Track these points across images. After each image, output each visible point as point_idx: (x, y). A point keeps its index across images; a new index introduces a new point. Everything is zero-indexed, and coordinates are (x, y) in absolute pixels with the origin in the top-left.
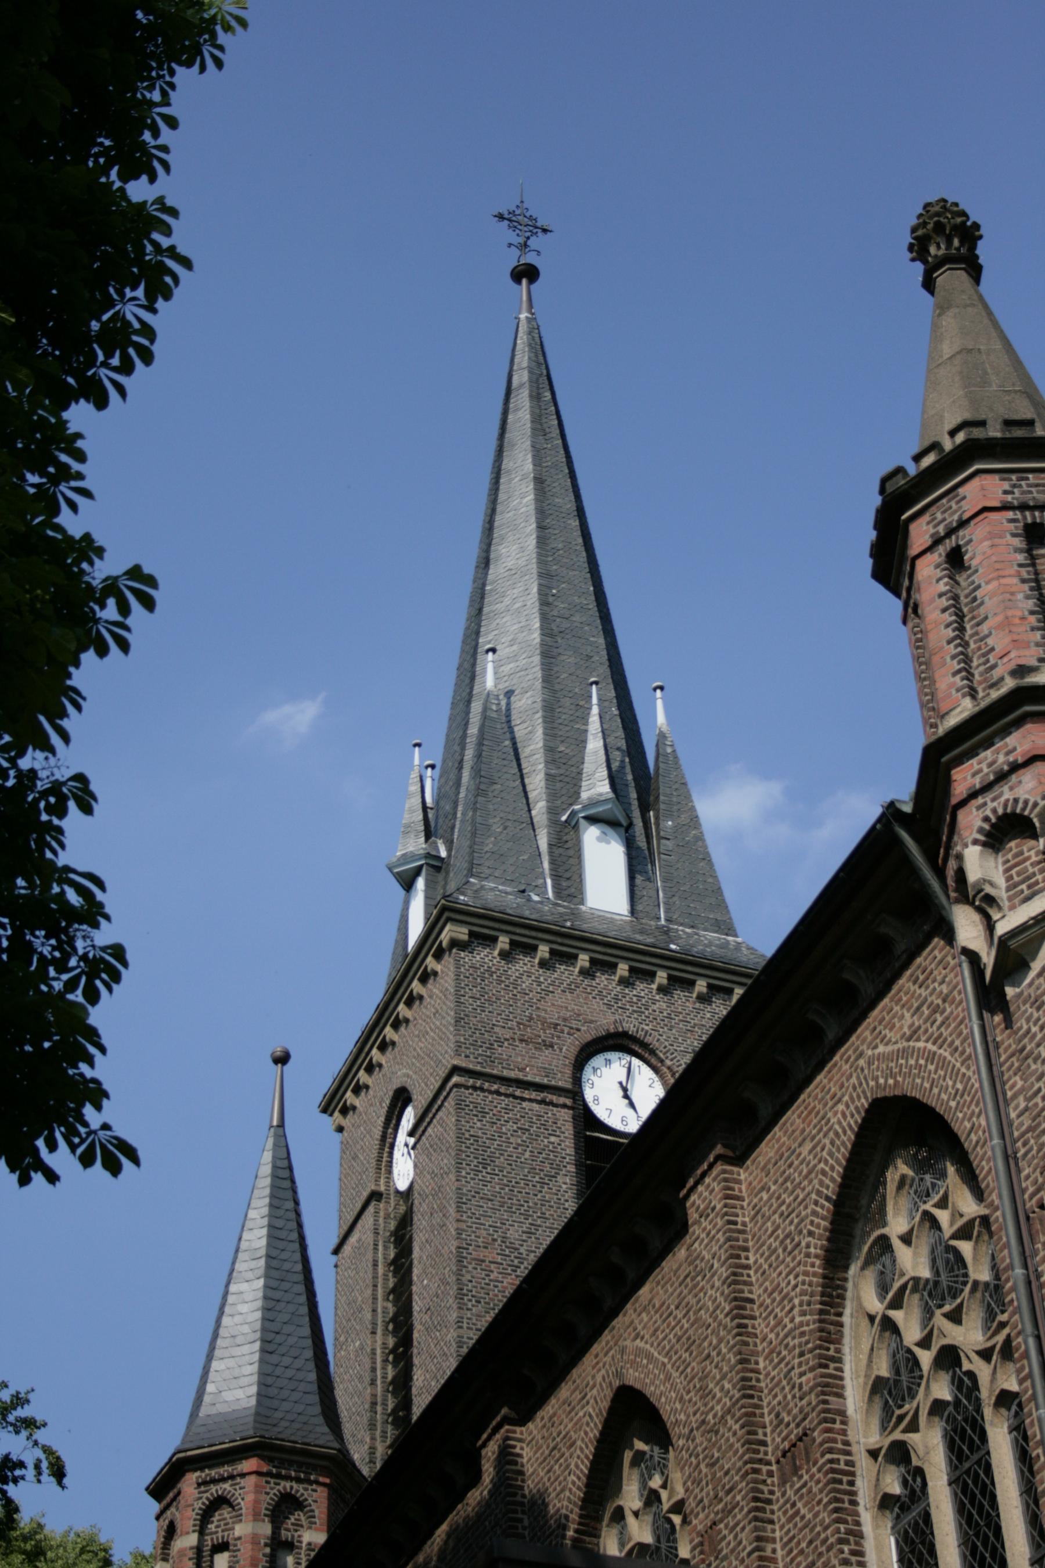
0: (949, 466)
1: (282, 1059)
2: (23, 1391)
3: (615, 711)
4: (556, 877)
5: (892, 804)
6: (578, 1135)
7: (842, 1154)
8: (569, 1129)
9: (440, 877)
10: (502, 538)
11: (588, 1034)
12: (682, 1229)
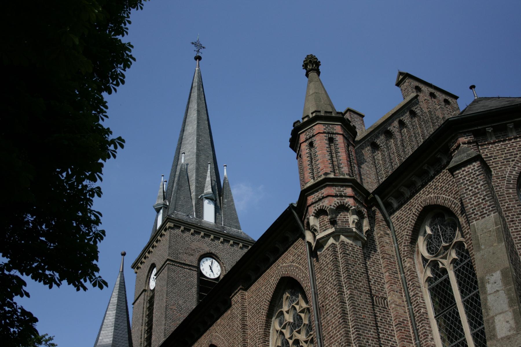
0: (311, 121)
1: (124, 254)
2: (52, 336)
3: (214, 171)
4: (196, 212)
5: (292, 204)
6: (198, 278)
7: (273, 290)
8: (196, 276)
9: (167, 210)
10: (188, 125)
11: (202, 253)
12: (230, 306)
